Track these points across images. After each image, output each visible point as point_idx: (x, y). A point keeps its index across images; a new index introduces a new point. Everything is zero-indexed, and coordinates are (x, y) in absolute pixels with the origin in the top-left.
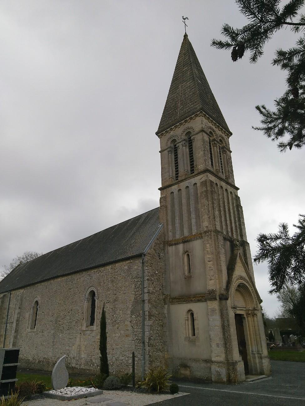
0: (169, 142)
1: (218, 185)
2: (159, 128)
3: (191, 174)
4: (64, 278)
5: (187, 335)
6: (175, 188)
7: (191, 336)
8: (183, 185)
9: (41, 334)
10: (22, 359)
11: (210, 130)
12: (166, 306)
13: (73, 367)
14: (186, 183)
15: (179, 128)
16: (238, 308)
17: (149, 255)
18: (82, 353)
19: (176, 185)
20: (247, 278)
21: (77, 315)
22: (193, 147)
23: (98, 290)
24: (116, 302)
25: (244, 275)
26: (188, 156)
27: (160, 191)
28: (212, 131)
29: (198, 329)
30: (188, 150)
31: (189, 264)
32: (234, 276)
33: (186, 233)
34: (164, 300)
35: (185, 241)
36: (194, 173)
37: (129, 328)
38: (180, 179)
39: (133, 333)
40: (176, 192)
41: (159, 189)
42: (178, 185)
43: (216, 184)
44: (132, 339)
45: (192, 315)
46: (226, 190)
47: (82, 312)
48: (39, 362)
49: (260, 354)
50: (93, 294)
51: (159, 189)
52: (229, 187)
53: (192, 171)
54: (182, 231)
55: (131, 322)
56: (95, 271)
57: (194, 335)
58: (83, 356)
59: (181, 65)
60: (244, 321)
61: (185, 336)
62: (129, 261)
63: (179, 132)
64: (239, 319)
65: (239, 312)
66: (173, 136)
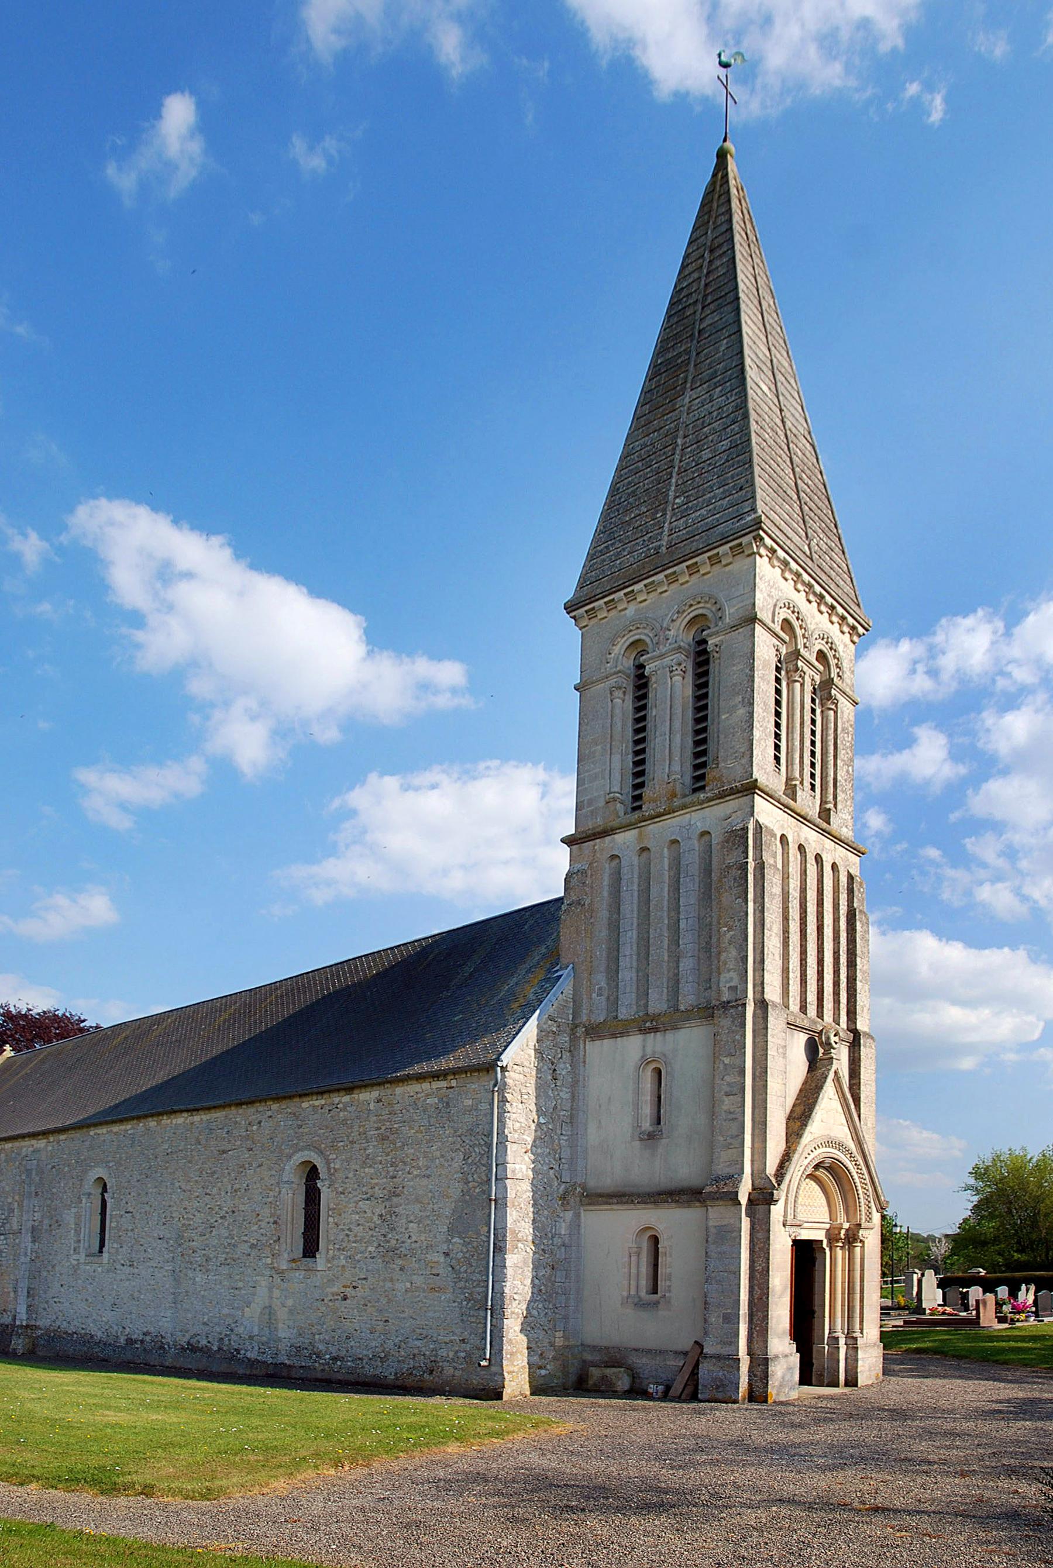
0: (618, 649)
1: (790, 840)
2: (581, 586)
3: (695, 790)
4: (197, 1118)
5: (632, 1293)
6: (625, 839)
7: (643, 1293)
8: (660, 832)
9: (127, 1270)
10: (66, 1333)
11: (784, 614)
12: (569, 1215)
13: (249, 1360)
14: (671, 826)
15: (661, 593)
16: (806, 1225)
17: (520, 1069)
18: (280, 1325)
19: (633, 832)
20: (852, 1146)
21: (255, 1228)
22: (711, 670)
23: (328, 1162)
24: (395, 1200)
25: (843, 1133)
26: (690, 714)
27: (566, 849)
28: (792, 618)
29: (669, 1277)
30: (689, 691)
31: (659, 1097)
32: (807, 1138)
33: (657, 1003)
34: (563, 1198)
35: (649, 1024)
36: (703, 788)
37: (440, 1272)
38: (648, 809)
39: (456, 1283)
40: (631, 861)
41: (569, 841)
42: (640, 834)
43: (783, 837)
44: (452, 1298)
45: (655, 1240)
46: (818, 858)
47: (272, 1220)
48: (130, 1342)
49: (856, 1339)
50: (312, 1173)
51: (569, 841)
52: (828, 844)
53: (699, 782)
54: (643, 994)
55: (446, 1254)
56: (317, 1103)
57: (655, 1290)
58: (281, 1335)
59: (695, 296)
60: (818, 1255)
61: (625, 1294)
62: (443, 1084)
63: (661, 606)
64: (806, 1255)
65: (805, 1235)
66: (636, 623)
